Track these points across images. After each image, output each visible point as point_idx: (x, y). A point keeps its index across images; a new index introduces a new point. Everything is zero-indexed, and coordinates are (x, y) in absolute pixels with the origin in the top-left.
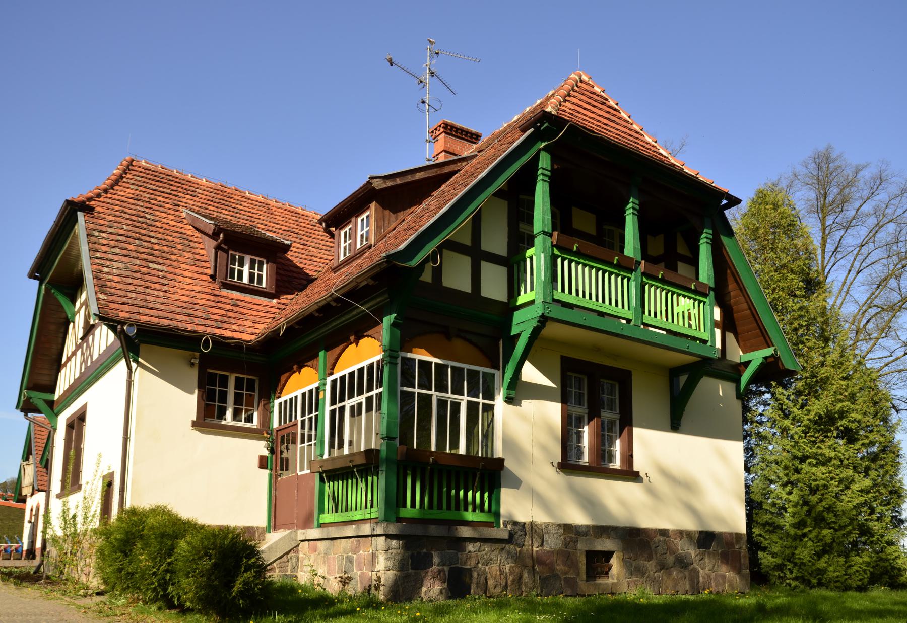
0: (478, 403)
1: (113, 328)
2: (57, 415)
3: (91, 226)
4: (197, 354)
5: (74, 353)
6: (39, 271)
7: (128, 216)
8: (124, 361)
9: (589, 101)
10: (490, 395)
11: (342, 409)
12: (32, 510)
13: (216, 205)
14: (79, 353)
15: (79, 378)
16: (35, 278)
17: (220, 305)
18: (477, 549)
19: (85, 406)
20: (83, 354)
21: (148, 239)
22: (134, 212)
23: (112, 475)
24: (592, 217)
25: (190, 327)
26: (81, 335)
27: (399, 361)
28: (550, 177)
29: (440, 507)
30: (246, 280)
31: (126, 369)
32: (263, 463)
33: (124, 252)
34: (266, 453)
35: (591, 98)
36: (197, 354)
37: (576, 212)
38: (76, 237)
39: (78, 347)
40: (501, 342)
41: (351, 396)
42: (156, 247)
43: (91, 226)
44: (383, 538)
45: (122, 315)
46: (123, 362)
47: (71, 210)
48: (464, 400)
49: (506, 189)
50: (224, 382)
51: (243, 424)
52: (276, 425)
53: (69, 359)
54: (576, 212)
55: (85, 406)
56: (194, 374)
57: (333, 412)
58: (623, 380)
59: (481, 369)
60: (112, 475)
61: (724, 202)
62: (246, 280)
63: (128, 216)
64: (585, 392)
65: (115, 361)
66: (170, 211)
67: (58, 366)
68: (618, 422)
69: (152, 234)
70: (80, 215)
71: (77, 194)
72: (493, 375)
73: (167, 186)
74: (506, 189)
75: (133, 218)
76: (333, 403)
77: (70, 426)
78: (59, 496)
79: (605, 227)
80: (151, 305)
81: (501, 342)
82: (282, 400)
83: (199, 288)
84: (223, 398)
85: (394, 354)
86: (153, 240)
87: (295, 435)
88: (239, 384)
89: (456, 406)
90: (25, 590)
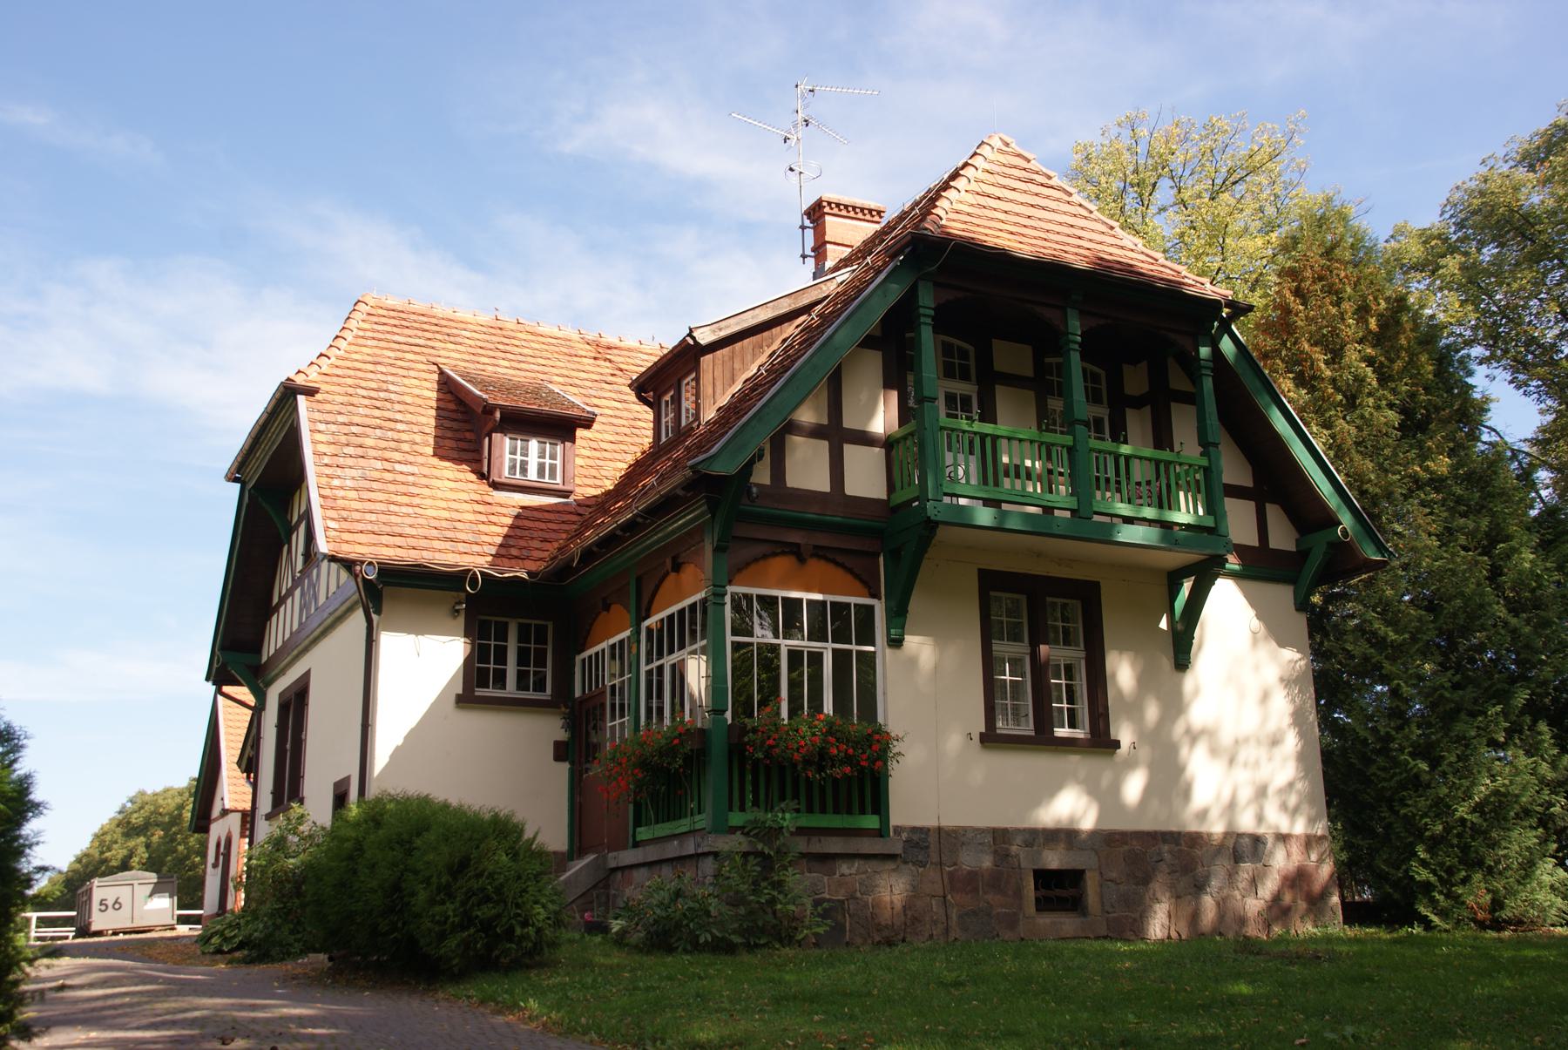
0: (850, 651)
2: (269, 684)
3: (317, 416)
4: (463, 595)
5: (290, 592)
7: (364, 393)
10: (867, 636)
11: (660, 669)
12: (218, 845)
13: (491, 353)
14: (298, 593)
15: (298, 631)
16: (236, 480)
17: (493, 518)
18: (853, 871)
19: (308, 674)
20: (302, 594)
21: (392, 425)
22: (374, 385)
23: (347, 780)
24: (1027, 351)
25: (451, 559)
27: (728, 599)
28: (934, 318)
30: (532, 474)
31: (365, 624)
32: (561, 752)
33: (360, 451)
34: (562, 735)
36: (463, 595)
39: (297, 583)
40: (881, 559)
41: (671, 651)
42: (404, 437)
43: (317, 416)
46: (359, 615)
47: (288, 395)
48: (827, 649)
50: (502, 635)
51: (530, 695)
52: (578, 693)
53: (282, 600)
55: (308, 674)
56: (461, 621)
57: (649, 673)
58: (1087, 597)
59: (853, 600)
60: (347, 780)
62: (532, 474)
63: (364, 393)
64: (1025, 621)
65: (351, 610)
68: (1083, 663)
69: (399, 416)
72: (872, 607)
73: (420, 334)
75: (373, 394)
76: (649, 661)
77: (283, 708)
78: (269, 817)
79: (1047, 360)
80: (397, 530)
81: (881, 559)
82: (586, 654)
83: (464, 496)
84: (501, 658)
85: (719, 590)
86: (400, 426)
87: (603, 705)
88: (523, 636)
89: (816, 658)
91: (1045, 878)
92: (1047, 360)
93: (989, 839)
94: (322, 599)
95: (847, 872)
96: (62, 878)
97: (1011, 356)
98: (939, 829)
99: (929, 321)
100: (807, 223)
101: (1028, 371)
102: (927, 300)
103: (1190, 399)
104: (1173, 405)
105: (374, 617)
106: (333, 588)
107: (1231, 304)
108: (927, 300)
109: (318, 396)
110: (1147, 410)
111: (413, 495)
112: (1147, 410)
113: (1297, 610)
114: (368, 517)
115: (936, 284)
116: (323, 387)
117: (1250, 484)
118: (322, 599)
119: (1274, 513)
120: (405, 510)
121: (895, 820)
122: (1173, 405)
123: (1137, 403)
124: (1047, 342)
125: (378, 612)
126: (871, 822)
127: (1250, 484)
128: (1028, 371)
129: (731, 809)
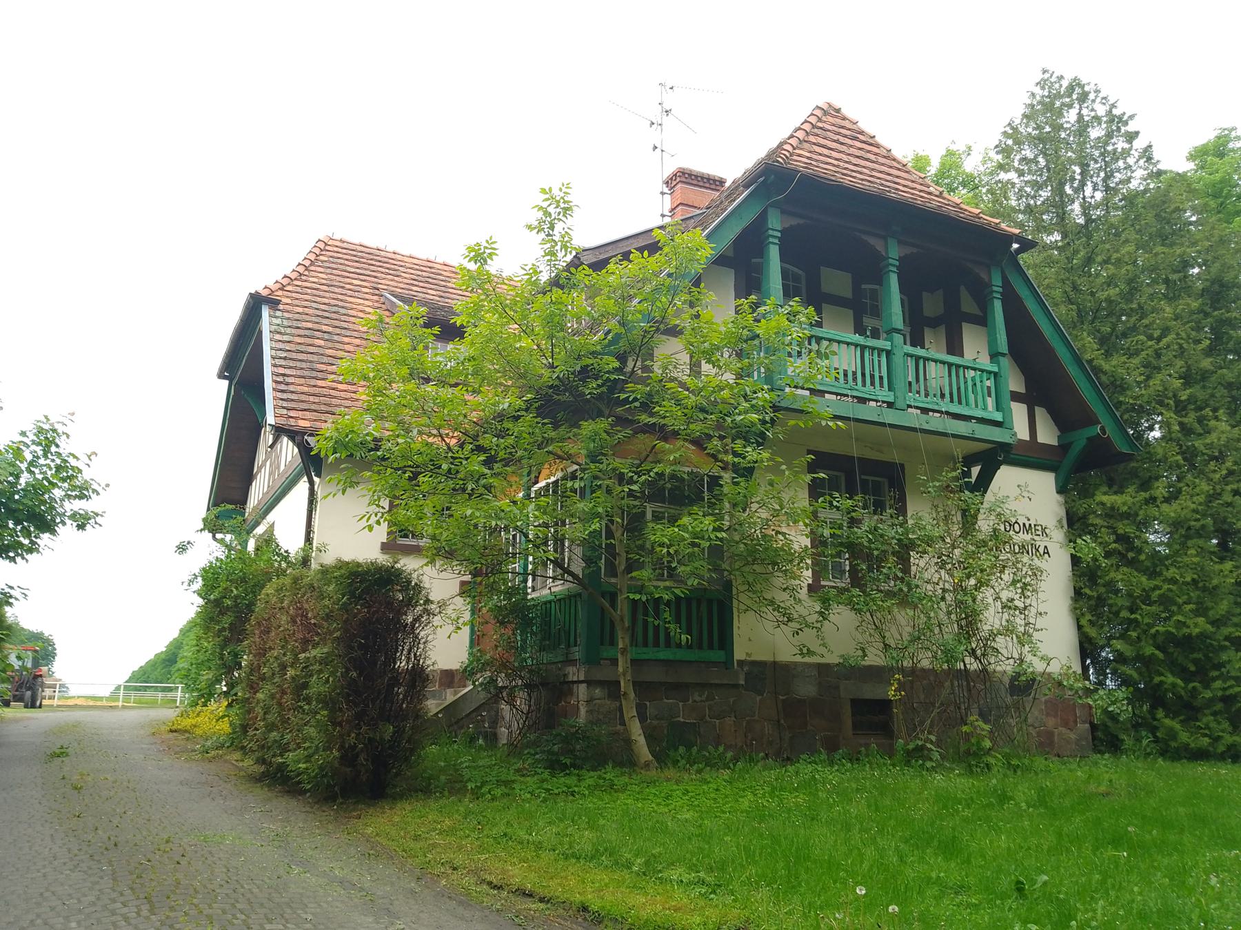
1: (292, 438)
5: (265, 462)
6: (229, 369)
8: (305, 478)
9: (836, 137)
16: (225, 378)
18: (704, 698)
26: (270, 442)
29: (656, 644)
35: (839, 134)
37: (825, 272)
38: (260, 332)
44: (584, 685)
45: (303, 423)
47: (255, 304)
49: (731, 254)
54: (825, 272)
61: (1015, 246)
65: (302, 476)
66: (367, 296)
67: (249, 477)
70: (265, 312)
71: (258, 287)
74: (731, 254)
79: (863, 286)
90: (906, 780)
91: (859, 705)
92: (863, 286)
93: (815, 673)
94: (282, 467)
95: (697, 698)
96: (198, 631)
97: (837, 281)
98: (775, 662)
99: (776, 241)
100: (666, 190)
101: (848, 293)
102: (775, 223)
103: (982, 320)
104: (964, 324)
105: (316, 479)
106: (289, 458)
107: (1018, 239)
108: (775, 223)
109: (281, 307)
110: (942, 330)
111: (285, 358)
112: (942, 330)
113: (1058, 492)
114: (311, 399)
115: (783, 212)
116: (285, 300)
117: (1023, 391)
118: (282, 467)
119: (1040, 412)
120: (343, 394)
121: (739, 654)
122: (964, 324)
123: (934, 323)
124: (868, 271)
125: (319, 475)
126: (717, 655)
127: (1023, 391)
128: (848, 293)
129: (602, 644)
